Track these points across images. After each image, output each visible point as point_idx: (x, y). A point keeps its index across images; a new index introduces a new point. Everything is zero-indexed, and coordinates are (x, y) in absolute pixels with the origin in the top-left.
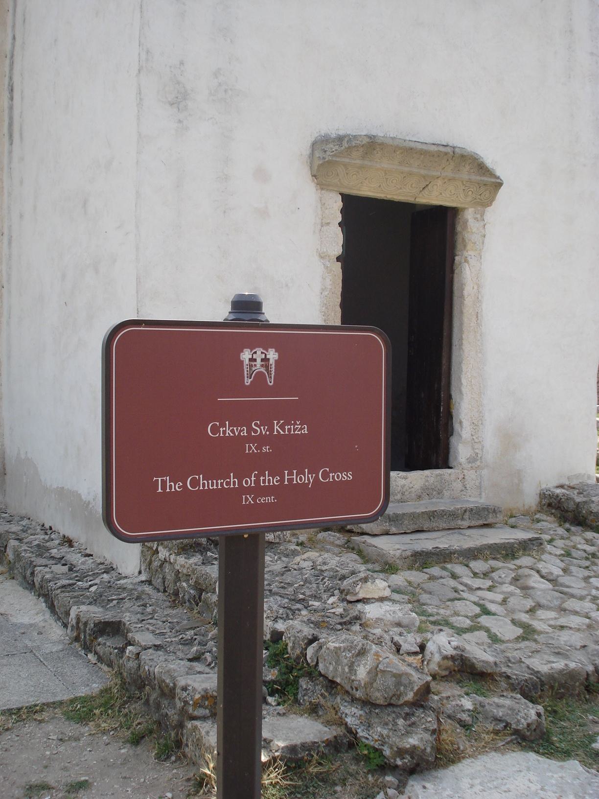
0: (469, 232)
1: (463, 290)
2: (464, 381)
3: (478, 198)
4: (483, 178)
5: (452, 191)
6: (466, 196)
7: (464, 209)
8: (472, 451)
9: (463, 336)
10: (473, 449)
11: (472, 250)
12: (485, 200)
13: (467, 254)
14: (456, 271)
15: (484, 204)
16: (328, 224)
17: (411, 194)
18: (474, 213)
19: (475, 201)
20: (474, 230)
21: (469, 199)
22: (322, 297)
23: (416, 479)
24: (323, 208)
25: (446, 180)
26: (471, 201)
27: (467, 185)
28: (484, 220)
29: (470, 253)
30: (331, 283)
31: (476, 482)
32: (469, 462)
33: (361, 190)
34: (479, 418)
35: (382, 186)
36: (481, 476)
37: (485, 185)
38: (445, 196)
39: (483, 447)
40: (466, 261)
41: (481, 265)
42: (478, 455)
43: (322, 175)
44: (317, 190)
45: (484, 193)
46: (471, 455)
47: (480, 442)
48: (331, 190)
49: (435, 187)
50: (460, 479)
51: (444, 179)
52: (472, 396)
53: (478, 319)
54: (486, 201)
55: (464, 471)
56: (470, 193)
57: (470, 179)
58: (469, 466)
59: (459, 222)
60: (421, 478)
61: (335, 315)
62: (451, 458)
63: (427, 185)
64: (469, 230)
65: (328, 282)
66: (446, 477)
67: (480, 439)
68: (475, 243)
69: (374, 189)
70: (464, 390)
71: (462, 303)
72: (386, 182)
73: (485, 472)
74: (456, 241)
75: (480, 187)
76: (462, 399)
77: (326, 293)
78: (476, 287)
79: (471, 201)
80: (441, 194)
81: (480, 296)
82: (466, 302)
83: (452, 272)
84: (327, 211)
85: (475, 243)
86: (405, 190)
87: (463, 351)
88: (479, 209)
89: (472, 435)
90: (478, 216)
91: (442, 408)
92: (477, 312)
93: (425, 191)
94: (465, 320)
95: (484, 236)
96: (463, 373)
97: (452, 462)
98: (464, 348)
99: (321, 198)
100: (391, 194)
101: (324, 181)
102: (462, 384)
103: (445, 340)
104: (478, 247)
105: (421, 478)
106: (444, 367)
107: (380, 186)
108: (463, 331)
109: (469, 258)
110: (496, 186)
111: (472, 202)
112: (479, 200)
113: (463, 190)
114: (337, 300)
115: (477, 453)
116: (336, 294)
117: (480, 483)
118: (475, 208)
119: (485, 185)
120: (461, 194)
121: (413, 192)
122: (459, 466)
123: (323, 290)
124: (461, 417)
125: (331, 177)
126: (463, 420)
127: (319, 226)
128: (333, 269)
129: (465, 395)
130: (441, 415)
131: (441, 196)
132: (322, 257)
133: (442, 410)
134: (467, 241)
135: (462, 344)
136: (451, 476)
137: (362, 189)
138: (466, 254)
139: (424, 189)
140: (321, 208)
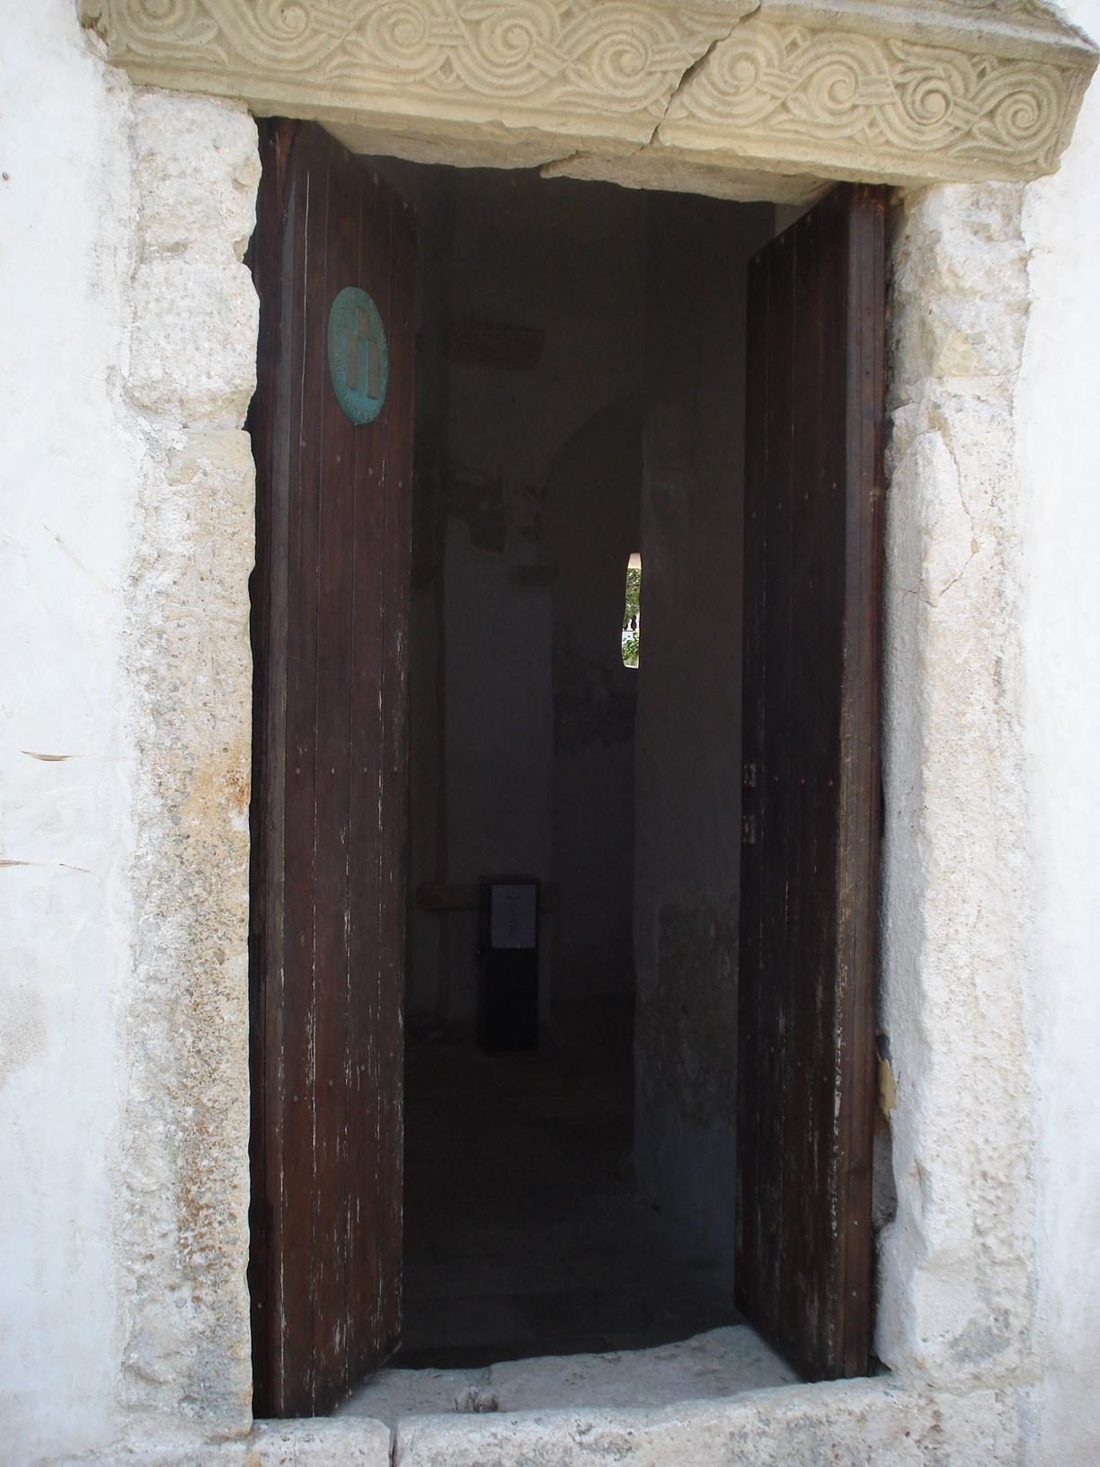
0: (945, 290)
1: (921, 555)
2: (934, 985)
3: (986, 134)
4: (989, 27)
5: (842, 93)
6: (919, 119)
7: (925, 188)
8: (981, 1305)
9: (928, 775)
10: (986, 1292)
11: (967, 370)
12: (1019, 139)
13: (939, 389)
14: (897, 477)
15: (1016, 161)
16: (178, 248)
17: (627, 109)
18: (968, 203)
19: (968, 144)
20: (972, 279)
21: (936, 135)
22: (141, 597)
23: (676, 1452)
24: (145, 177)
25: (795, 34)
26: (949, 146)
27: (913, 62)
28: (1019, 237)
29: (953, 385)
30: (188, 528)
31: (1001, 1441)
32: (964, 1357)
33: (354, 91)
34: (1015, 1151)
35: (456, 64)
36: (1023, 1414)
37: (1005, 61)
38: (804, 116)
39: (1033, 1283)
40: (938, 423)
41: (1011, 439)
42: (1012, 1319)
43: (120, 14)
44: (110, 90)
45: (1008, 109)
46: (972, 1322)
47: (1018, 1258)
48: (193, 93)
49: (745, 69)
50: (915, 1436)
51: (781, 25)
52: (981, 1051)
53: (1002, 693)
54: (1025, 146)
55: (939, 1397)
56: (936, 102)
57: (918, 27)
58: (962, 1376)
59: (907, 254)
60: (707, 1446)
61: (218, 682)
62: (886, 1328)
63: (702, 62)
64: (947, 280)
65: (175, 527)
66: (844, 1430)
67: (1022, 1248)
68: (977, 340)
69: (423, 82)
70: (935, 1023)
71: (920, 619)
72: (479, 48)
73: (1042, 1396)
74: (898, 342)
75: (982, 74)
76: (925, 1066)
77: (165, 579)
78: (988, 543)
79: (949, 146)
80: (784, 105)
81: (1009, 582)
82: (935, 614)
83: (882, 480)
84: (168, 191)
85: (977, 340)
86: (585, 87)
87: (928, 842)
88: (995, 185)
89: (979, 1231)
90: (994, 219)
91: (838, 1101)
92: (999, 661)
93: (694, 87)
94: (936, 697)
95: (1025, 309)
96: (930, 946)
97: (889, 1355)
98: (930, 826)
99: (133, 126)
100: (521, 111)
101: (142, 41)
102: (922, 996)
103: (851, 792)
104: (992, 356)
105: (707, 1446)
106: (848, 913)
107: (447, 67)
108: (927, 751)
109: (948, 411)
110: (1063, 70)
111: (952, 152)
112: (986, 143)
113: (897, 86)
114: (228, 612)
115: (1006, 1312)
116: (221, 582)
117: (1021, 1444)
118: (970, 180)
119: (1005, 61)
120: (890, 112)
121: (630, 94)
122: (915, 1372)
123: (145, 563)
124: (919, 1150)
125: (171, 20)
126: (928, 1166)
127: (124, 261)
128: (205, 463)
129: (937, 1046)
130: (836, 1132)
131: (784, 116)
132: (144, 408)
133: (837, 1113)
134: (939, 331)
135: (922, 808)
136: (871, 1425)
137: (359, 85)
138: (934, 389)
139: (689, 74)
140: (134, 173)
